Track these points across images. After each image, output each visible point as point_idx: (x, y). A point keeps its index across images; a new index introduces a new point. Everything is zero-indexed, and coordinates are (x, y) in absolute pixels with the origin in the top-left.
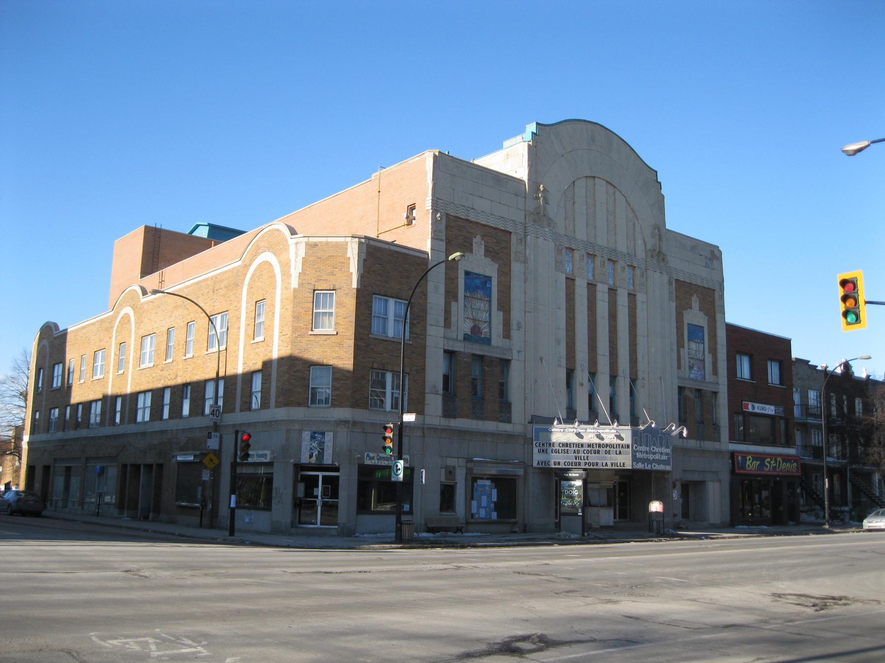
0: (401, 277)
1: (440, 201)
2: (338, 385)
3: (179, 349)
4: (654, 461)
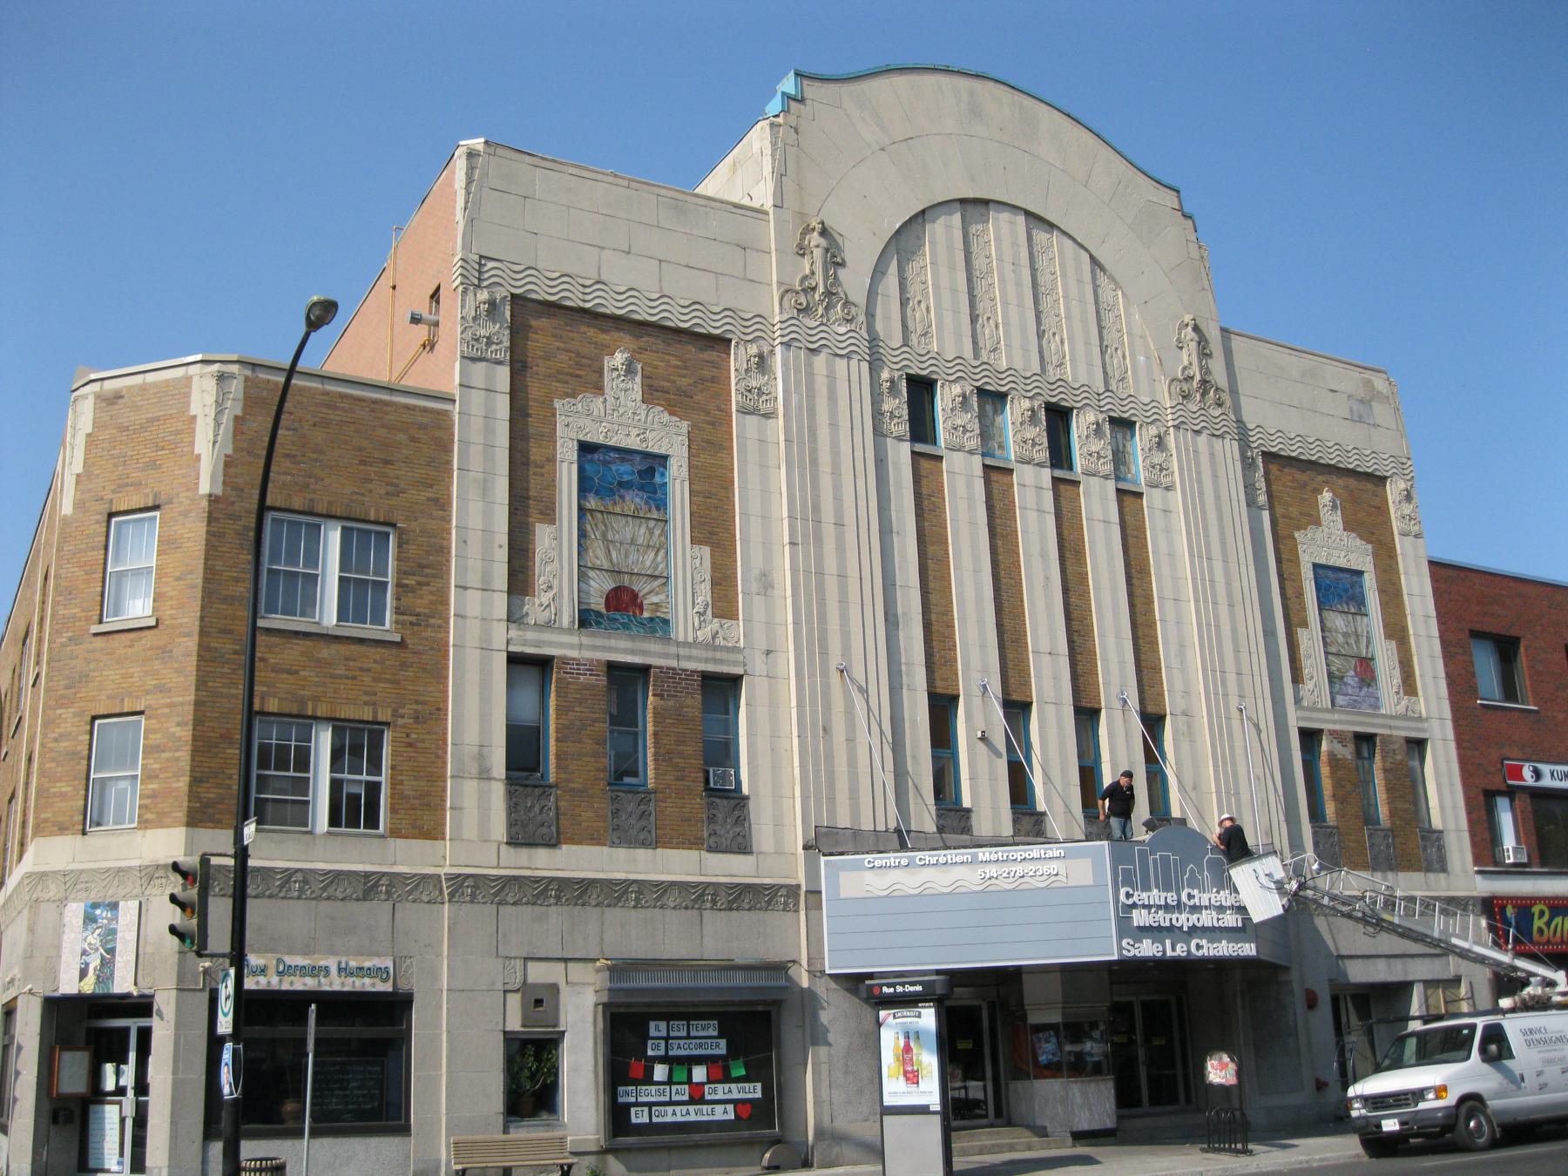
0: (363, 463)
2: (156, 766)
4: (1194, 930)
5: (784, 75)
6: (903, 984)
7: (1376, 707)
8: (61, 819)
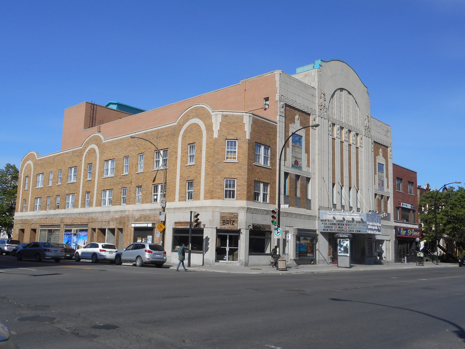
0: (267, 135)
1: (283, 97)
3: (133, 168)
5: (320, 59)
7: (383, 190)
8: (219, 196)
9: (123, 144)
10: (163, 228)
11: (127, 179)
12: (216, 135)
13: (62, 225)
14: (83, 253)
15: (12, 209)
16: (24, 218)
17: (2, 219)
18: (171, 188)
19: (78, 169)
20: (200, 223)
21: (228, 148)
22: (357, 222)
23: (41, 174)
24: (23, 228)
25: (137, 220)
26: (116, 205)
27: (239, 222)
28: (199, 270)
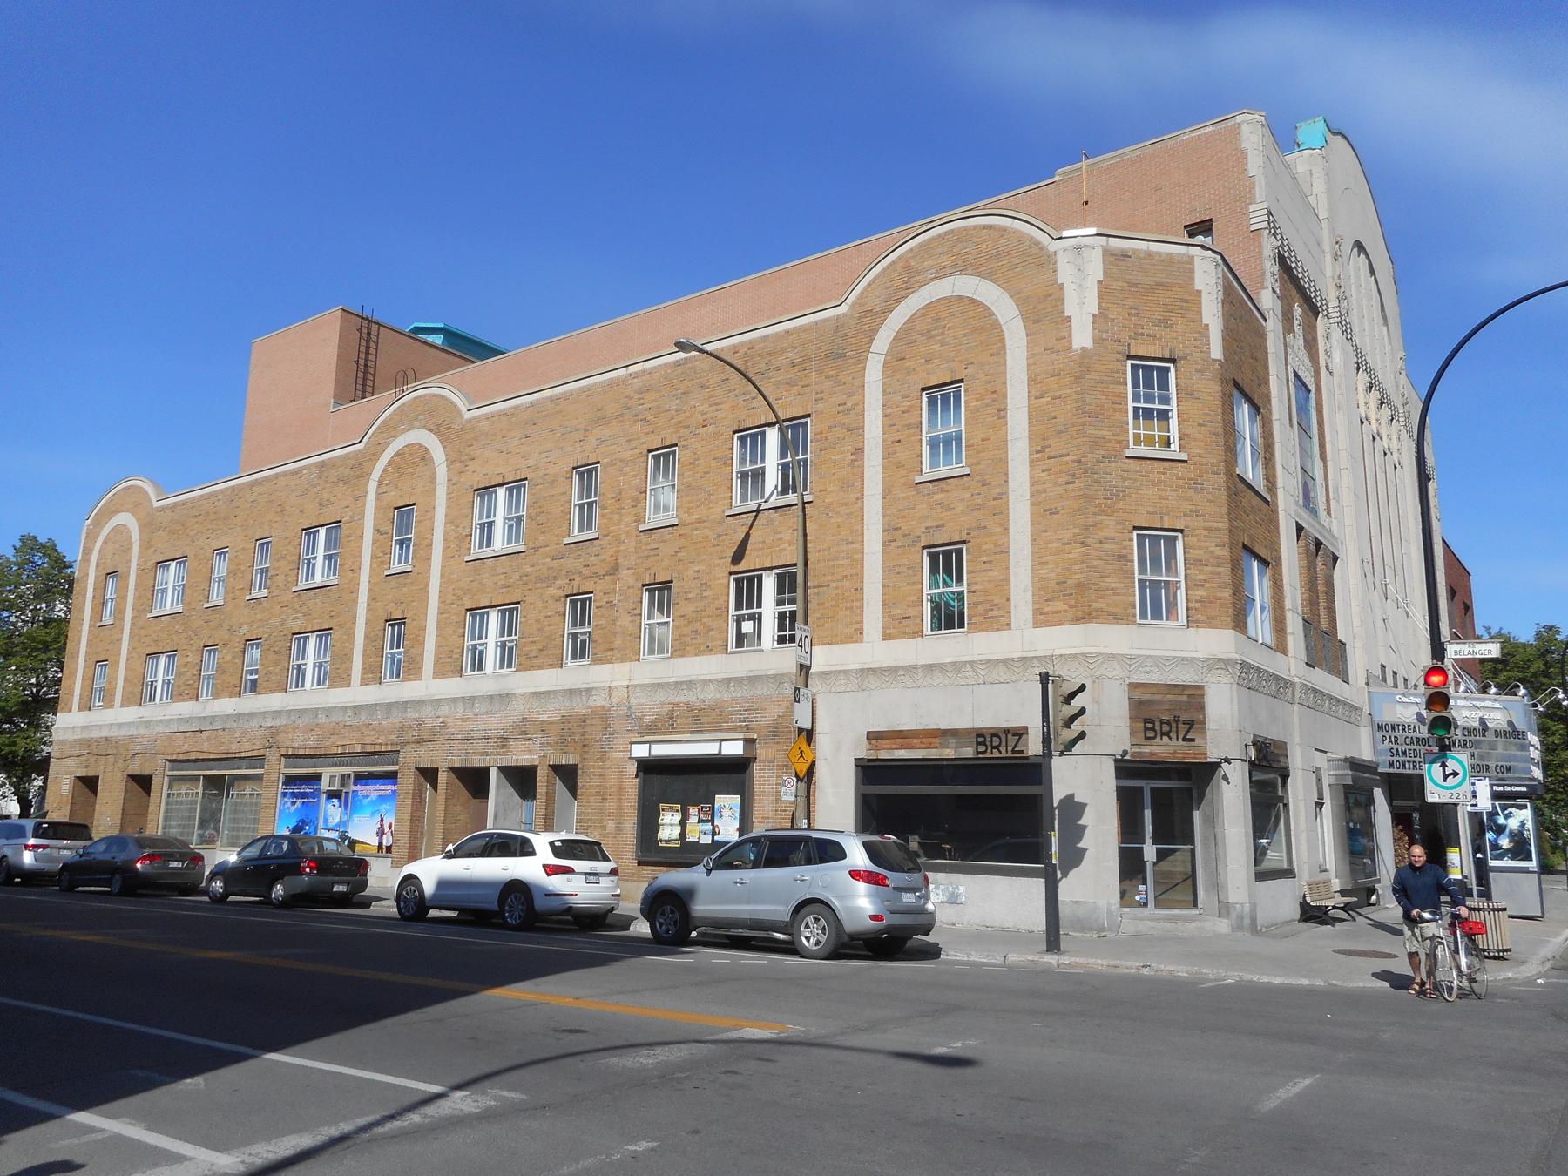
6: (1511, 786)
9: (564, 417)
10: (810, 762)
11: (593, 558)
12: (1082, 337)
13: (273, 758)
14: (443, 884)
15: (41, 705)
16: (96, 734)
17: (4, 738)
18: (833, 585)
19: (344, 531)
20: (1020, 735)
21: (1136, 398)
22: (1497, 733)
23: (173, 560)
24: (91, 774)
25: (650, 730)
26: (540, 667)
27: (1211, 725)
28: (1146, 971)
